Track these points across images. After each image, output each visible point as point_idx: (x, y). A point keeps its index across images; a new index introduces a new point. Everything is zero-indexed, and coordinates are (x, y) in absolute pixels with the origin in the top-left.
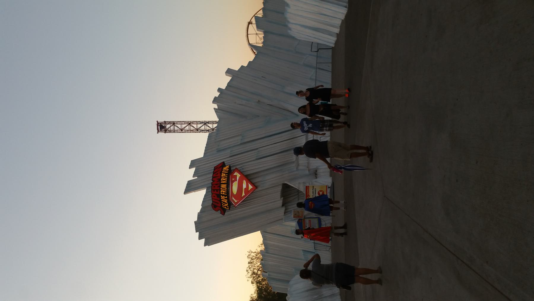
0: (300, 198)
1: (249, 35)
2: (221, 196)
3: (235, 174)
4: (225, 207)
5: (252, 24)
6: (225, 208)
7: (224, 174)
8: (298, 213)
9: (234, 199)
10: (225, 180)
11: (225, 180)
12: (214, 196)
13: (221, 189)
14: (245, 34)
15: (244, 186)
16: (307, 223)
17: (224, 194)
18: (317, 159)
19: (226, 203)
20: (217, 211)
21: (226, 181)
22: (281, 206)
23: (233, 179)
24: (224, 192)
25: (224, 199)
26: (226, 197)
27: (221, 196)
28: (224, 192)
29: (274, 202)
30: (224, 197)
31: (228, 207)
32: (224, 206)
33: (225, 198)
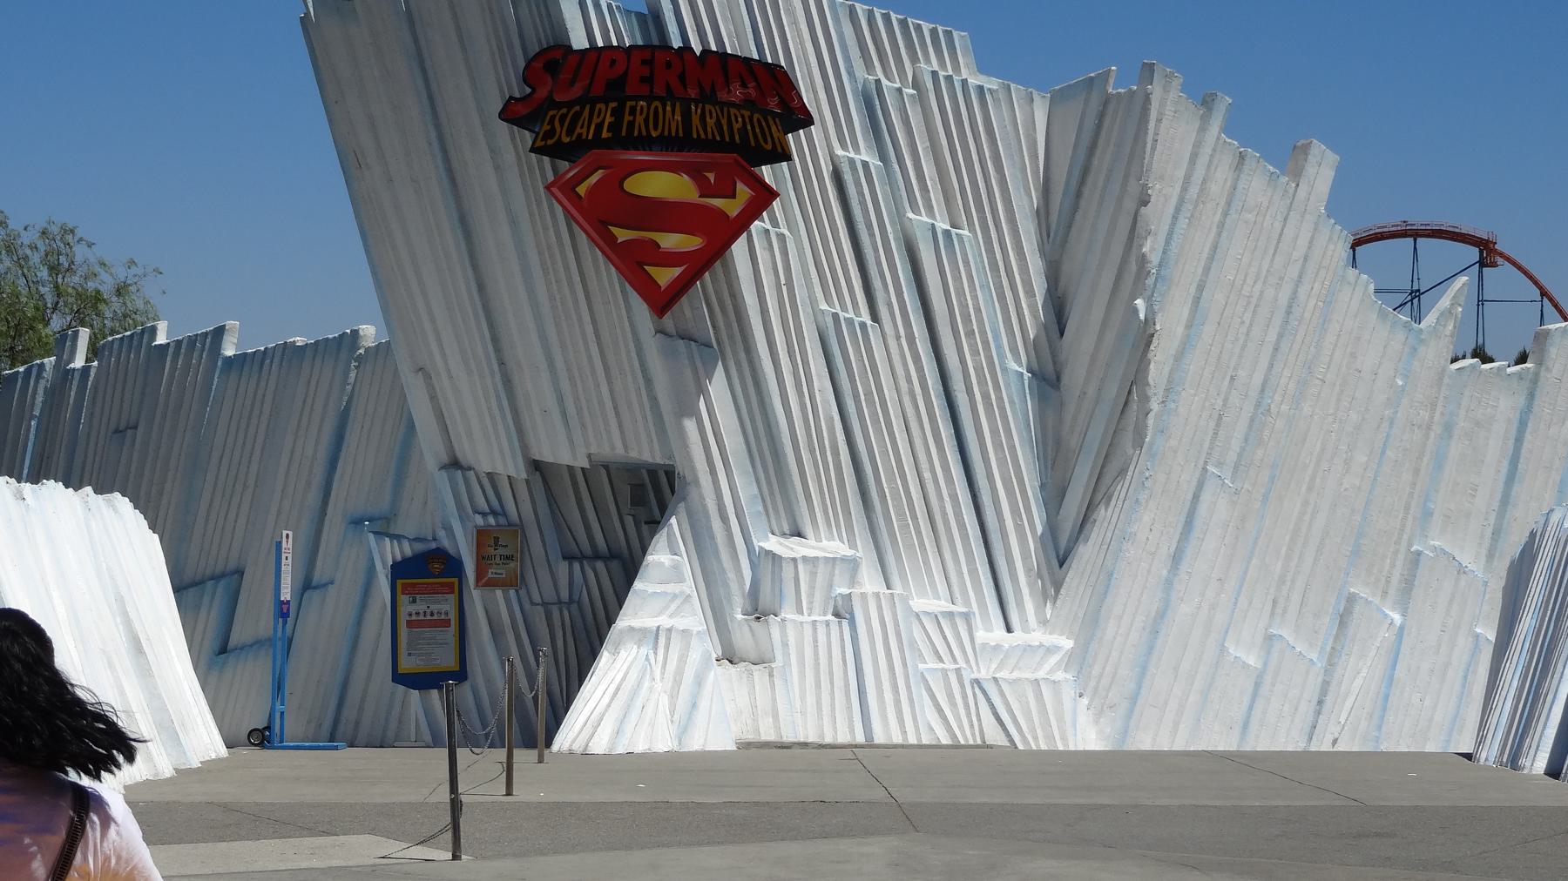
0: (577, 566)
1: (1411, 240)
2: (613, 105)
3: (740, 187)
4: (551, 122)
5: (1482, 263)
6: (546, 127)
7: (740, 125)
8: (507, 558)
9: (594, 179)
10: (706, 133)
11: (706, 133)
12: (613, 62)
13: (656, 103)
14: (1418, 219)
15: (670, 241)
16: (435, 607)
17: (627, 118)
18: (127, 499)
19: (569, 133)
20: (528, 77)
21: (703, 136)
22: (537, 458)
23: (711, 177)
24: (640, 119)
25: (596, 120)
26: (605, 134)
27: (613, 105)
28: (640, 119)
29: (564, 414)
30: (609, 119)
31: (550, 142)
32: (553, 117)
33: (599, 127)
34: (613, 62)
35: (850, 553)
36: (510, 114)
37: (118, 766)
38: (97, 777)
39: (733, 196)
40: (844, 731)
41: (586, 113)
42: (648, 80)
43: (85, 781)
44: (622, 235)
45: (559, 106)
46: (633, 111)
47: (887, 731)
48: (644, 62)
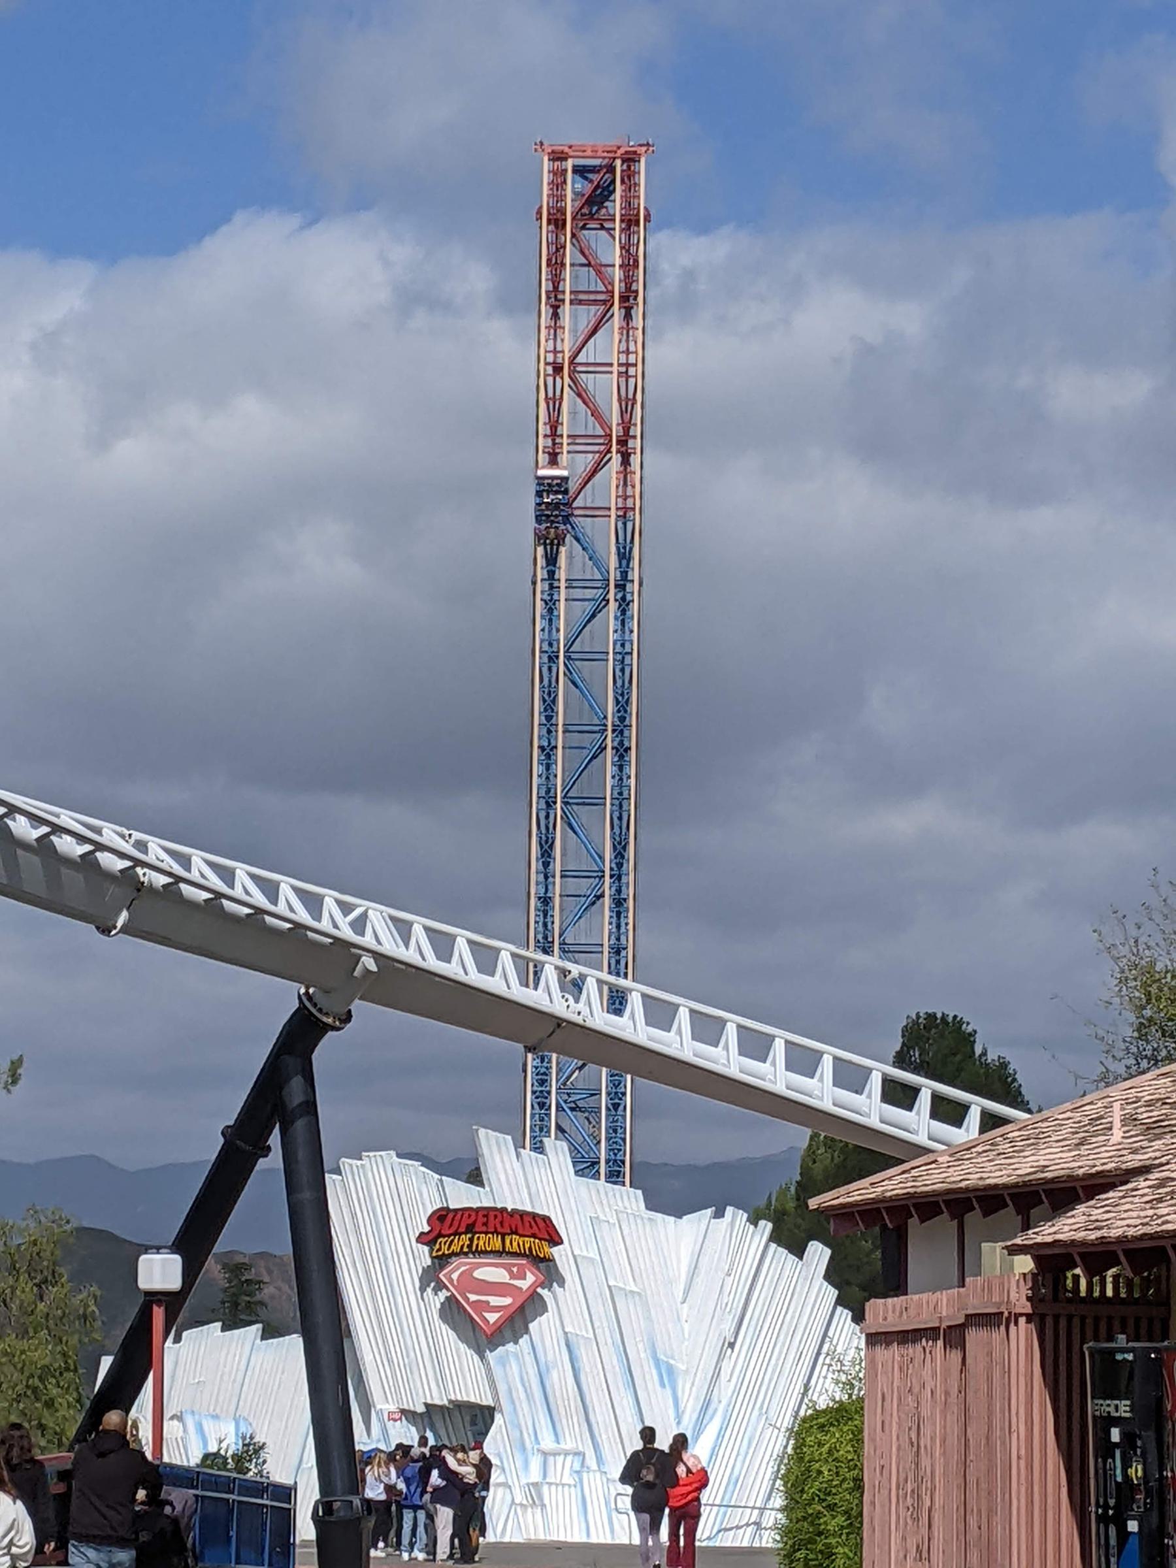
12: (470, 1216)
15: (495, 1301)
24: (481, 1243)
28: (481, 1243)
30: (468, 1242)
34: (470, 1216)
35: (1105, 1319)
36: (422, 1238)
37: (955, 1017)
38: (286, 1493)
39: (524, 1278)
40: (584, 1540)
41: (456, 1240)
42: (485, 1224)
43: (651, 1446)
44: (473, 1297)
45: (444, 1236)
46: (479, 1238)
47: (594, 1540)
48: (484, 1216)
